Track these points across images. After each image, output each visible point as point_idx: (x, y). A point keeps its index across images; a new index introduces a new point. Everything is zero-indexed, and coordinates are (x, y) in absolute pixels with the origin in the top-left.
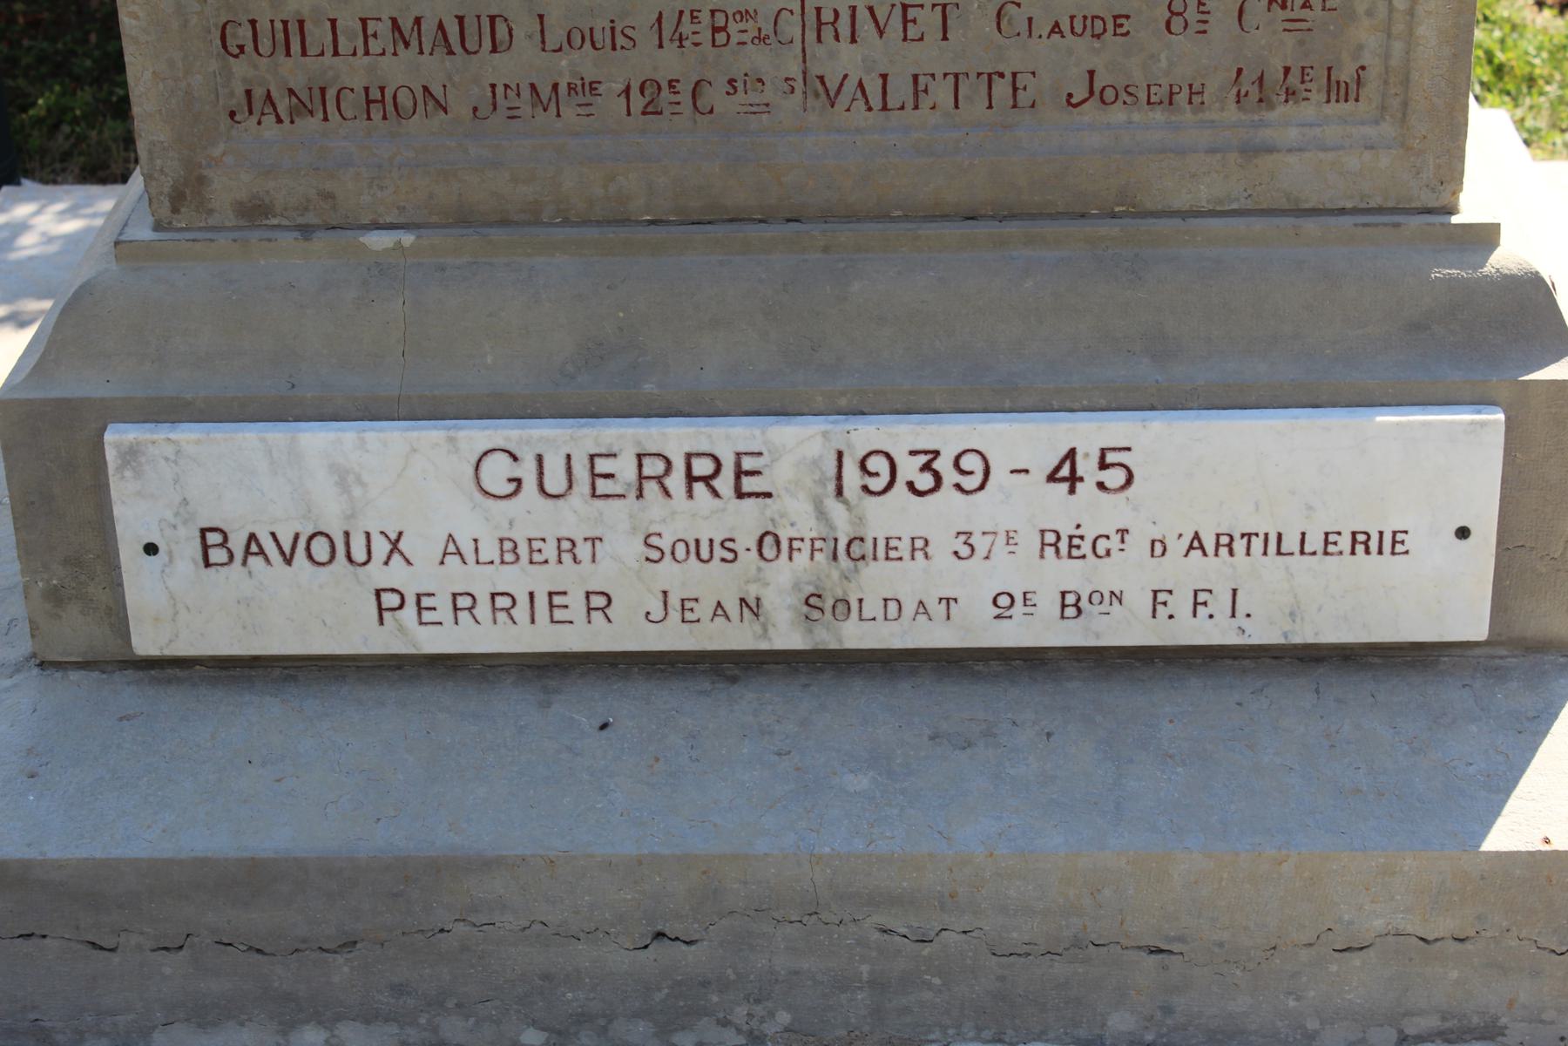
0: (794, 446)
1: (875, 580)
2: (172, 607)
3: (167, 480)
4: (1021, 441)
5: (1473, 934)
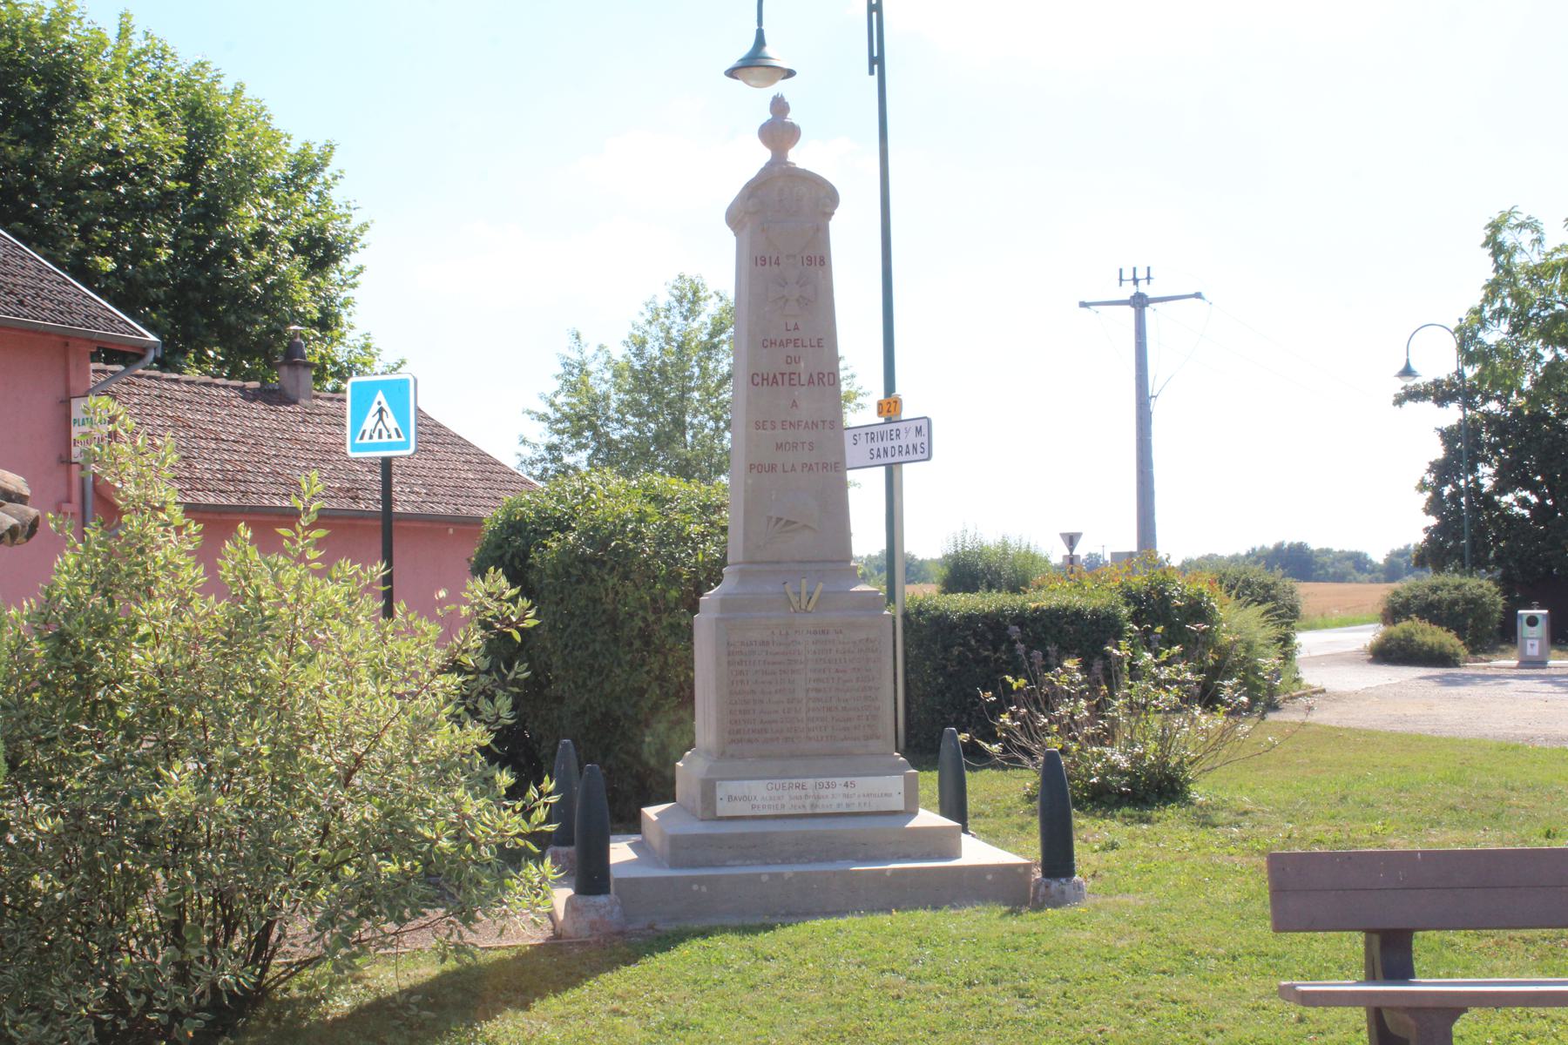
0: (810, 782)
1: (821, 802)
2: (723, 808)
3: (724, 789)
4: (840, 781)
5: (755, 102)
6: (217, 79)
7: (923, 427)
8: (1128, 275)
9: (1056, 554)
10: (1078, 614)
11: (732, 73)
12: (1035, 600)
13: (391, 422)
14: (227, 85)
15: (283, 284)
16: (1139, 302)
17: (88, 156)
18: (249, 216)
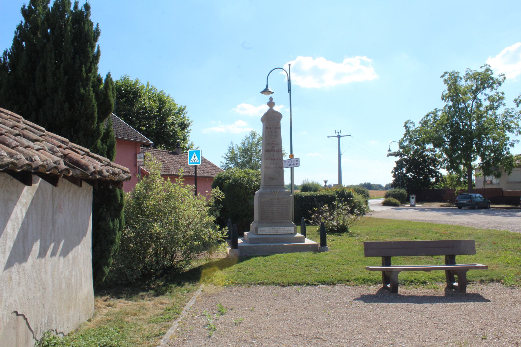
6: (165, 94)
7: (298, 160)
8: (337, 131)
9: (323, 185)
10: (327, 196)
11: (262, 92)
12: (319, 193)
13: (197, 158)
14: (166, 95)
15: (176, 132)
16: (339, 137)
17: (141, 108)
18: (170, 119)
